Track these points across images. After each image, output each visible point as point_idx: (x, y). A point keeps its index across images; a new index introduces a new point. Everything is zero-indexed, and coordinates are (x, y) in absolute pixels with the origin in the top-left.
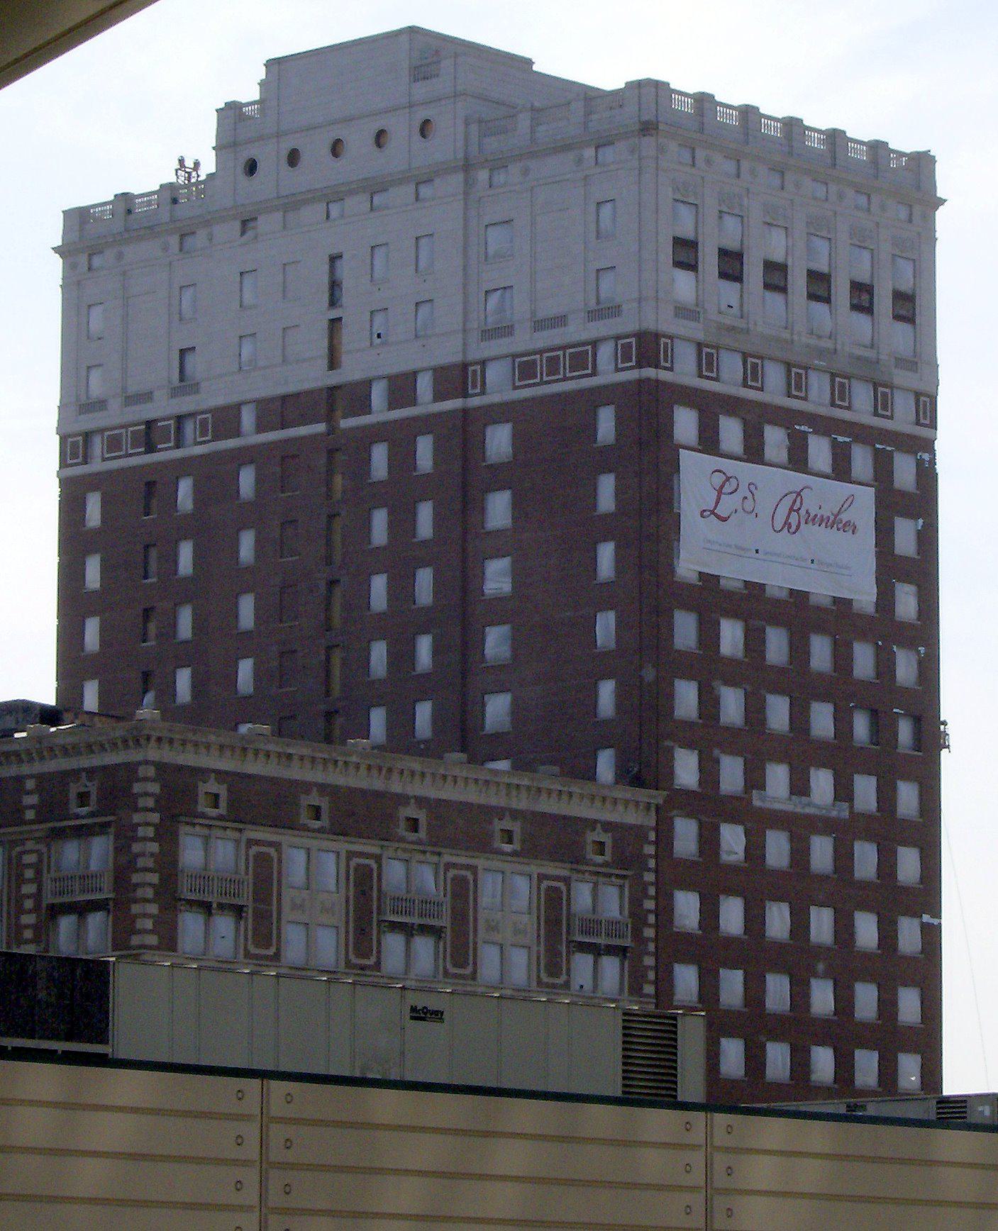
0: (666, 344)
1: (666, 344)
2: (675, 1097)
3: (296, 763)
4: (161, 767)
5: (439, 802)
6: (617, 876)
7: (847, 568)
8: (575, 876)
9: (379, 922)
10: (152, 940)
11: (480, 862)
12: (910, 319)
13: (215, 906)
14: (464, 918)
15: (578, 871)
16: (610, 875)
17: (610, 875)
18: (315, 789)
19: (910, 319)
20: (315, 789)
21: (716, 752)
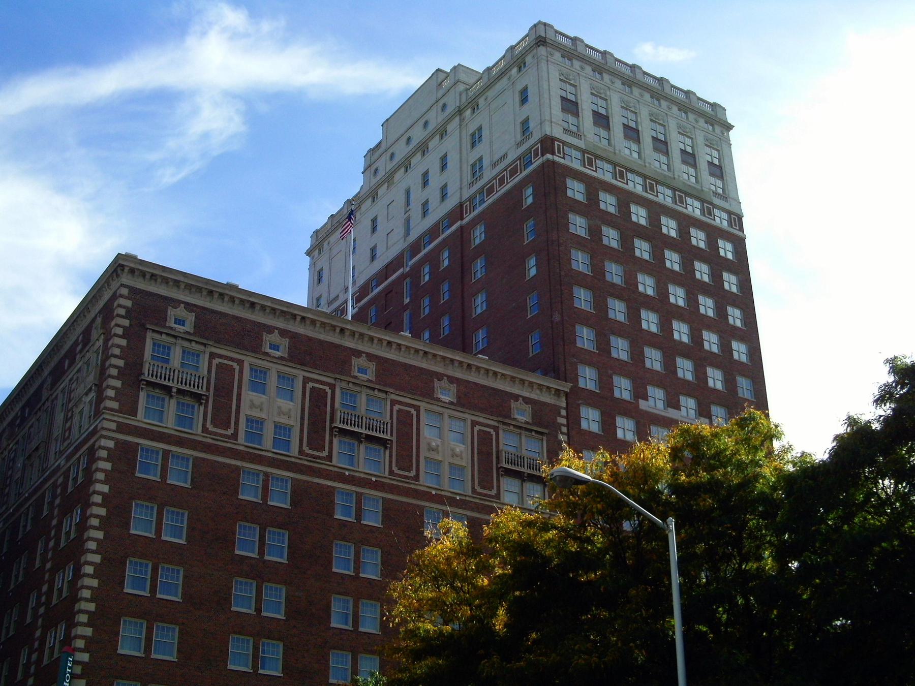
0: (559, 146)
1: (559, 146)
2: (167, 361)
3: (376, 392)
4: (133, 291)
5: (387, 360)
6: (537, 432)
7: (592, 94)
8: (501, 426)
9: (332, 429)
10: (115, 405)
11: (423, 405)
12: (721, 177)
13: (174, 390)
14: (153, 276)
15: (504, 423)
16: (531, 431)
17: (531, 431)
18: (276, 331)
19: (721, 177)
20: (276, 331)
21: (610, 372)
